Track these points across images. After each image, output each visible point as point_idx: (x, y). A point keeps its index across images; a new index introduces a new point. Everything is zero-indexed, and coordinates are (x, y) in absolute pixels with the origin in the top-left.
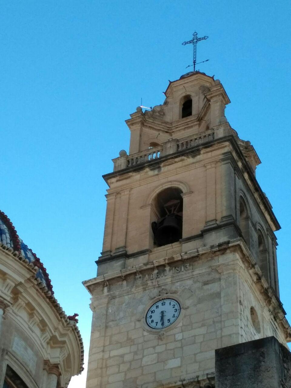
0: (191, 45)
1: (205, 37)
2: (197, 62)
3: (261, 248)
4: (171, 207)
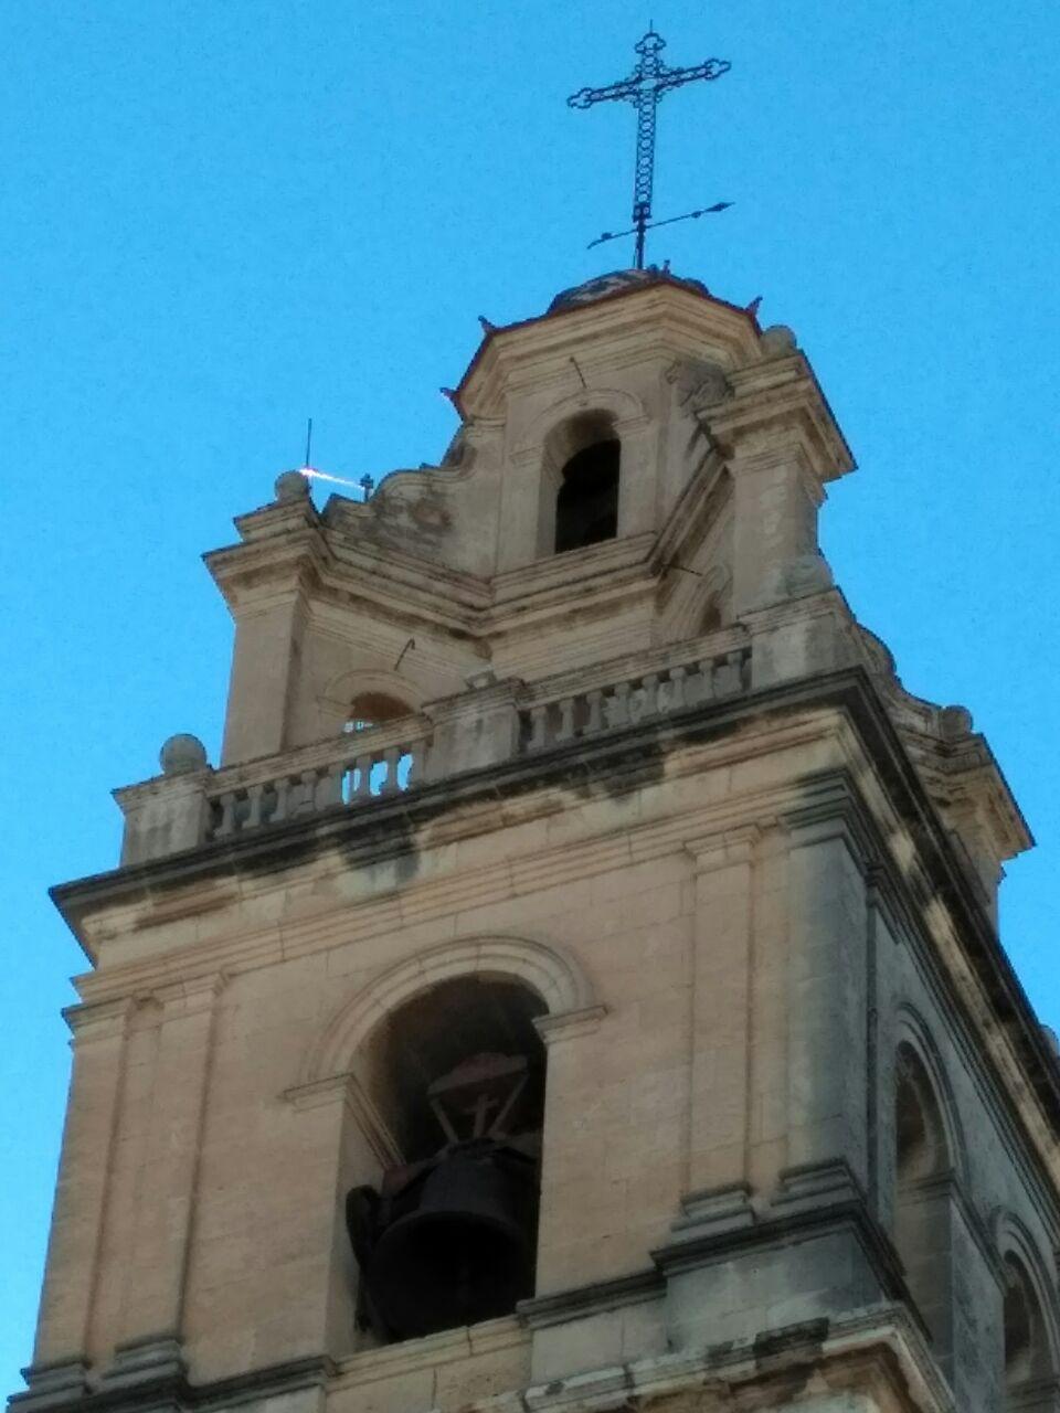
0: (623, 113)
1: (707, 66)
2: (657, 212)
3: (1023, 1373)
4: (468, 1094)
